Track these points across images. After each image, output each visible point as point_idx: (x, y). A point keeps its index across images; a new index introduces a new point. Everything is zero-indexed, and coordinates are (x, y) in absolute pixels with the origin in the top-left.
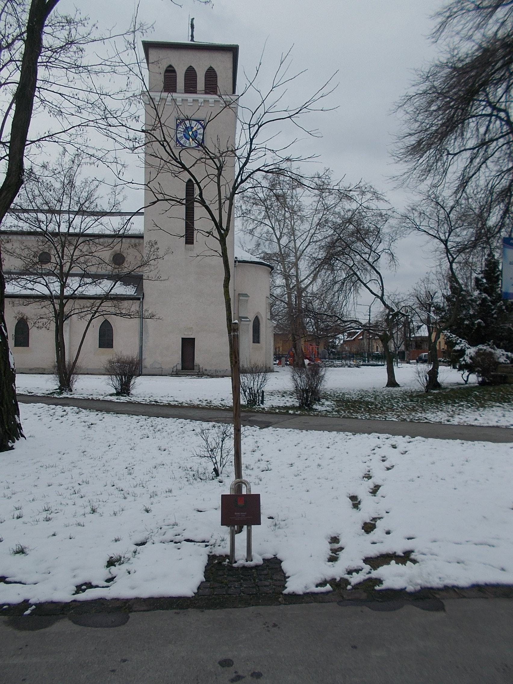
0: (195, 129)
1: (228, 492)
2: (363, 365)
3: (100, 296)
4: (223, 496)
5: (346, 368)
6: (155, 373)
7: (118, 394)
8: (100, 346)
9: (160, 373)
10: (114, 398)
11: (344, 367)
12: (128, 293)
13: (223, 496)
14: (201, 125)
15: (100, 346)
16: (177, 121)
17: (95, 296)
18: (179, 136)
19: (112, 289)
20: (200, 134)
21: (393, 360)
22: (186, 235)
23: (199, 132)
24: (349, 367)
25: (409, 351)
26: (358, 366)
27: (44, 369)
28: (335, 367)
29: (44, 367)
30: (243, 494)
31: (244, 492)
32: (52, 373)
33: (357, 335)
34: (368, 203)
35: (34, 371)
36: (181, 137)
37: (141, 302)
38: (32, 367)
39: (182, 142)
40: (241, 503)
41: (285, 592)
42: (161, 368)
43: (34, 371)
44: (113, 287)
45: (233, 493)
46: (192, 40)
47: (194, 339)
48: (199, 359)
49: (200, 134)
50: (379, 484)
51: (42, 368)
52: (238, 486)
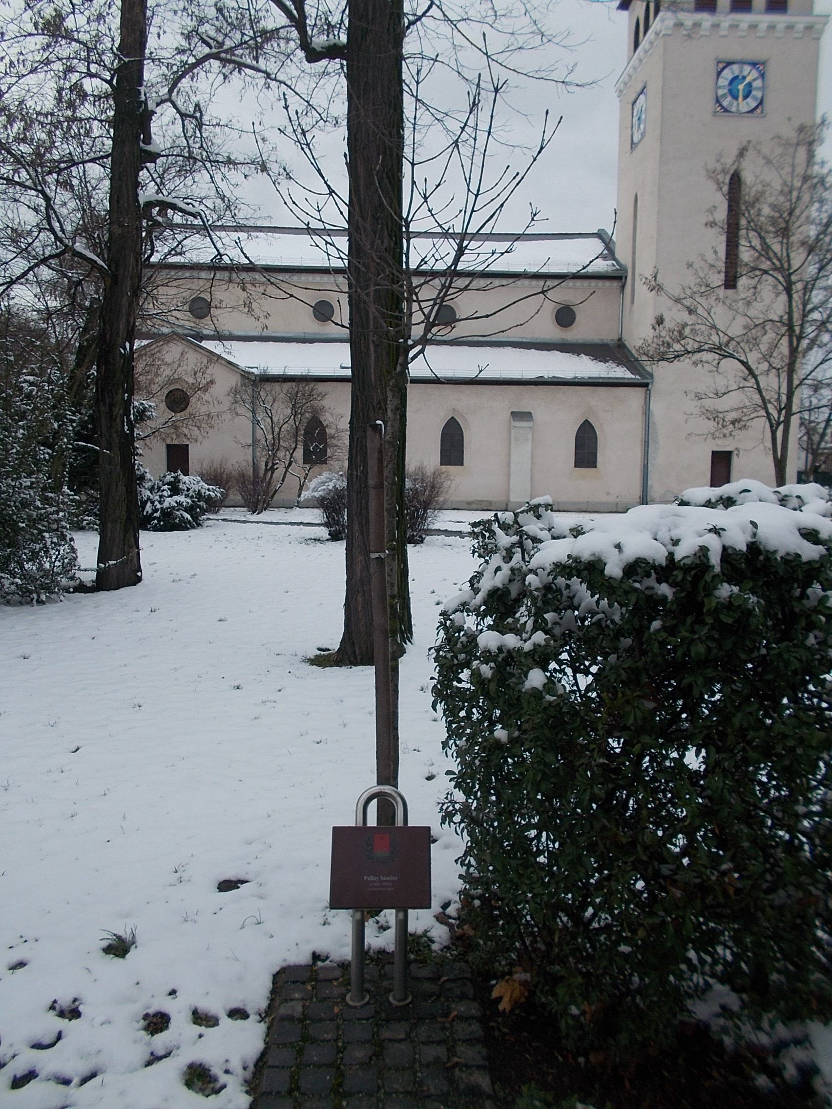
0: (748, 80)
1: (349, 820)
4: (339, 833)
13: (339, 833)
27: (490, 503)
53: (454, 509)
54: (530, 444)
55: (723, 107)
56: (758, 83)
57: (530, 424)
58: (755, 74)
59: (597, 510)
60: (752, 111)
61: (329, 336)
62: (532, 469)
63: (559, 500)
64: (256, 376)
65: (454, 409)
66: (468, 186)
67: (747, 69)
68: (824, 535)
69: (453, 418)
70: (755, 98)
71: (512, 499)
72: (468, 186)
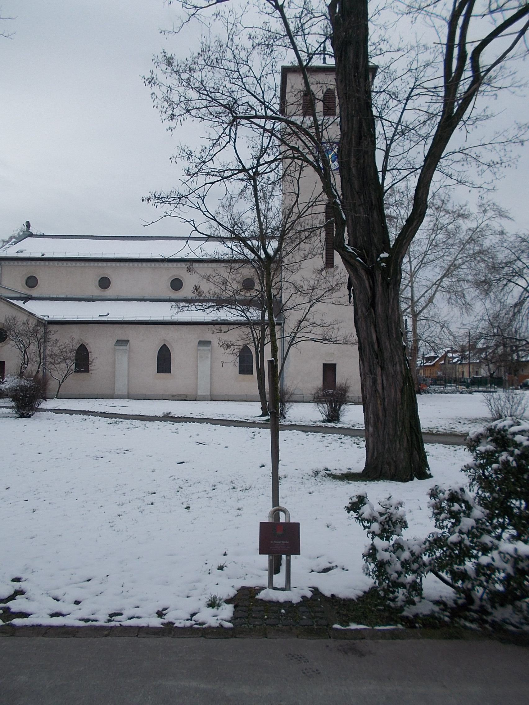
1: (266, 520)
2: (476, 391)
3: (241, 322)
4: (262, 524)
5: (458, 395)
7: (329, 421)
10: (322, 424)
11: (456, 393)
13: (262, 524)
17: (237, 322)
19: (306, 315)
24: (461, 393)
25: (518, 377)
27: (186, 396)
28: (445, 393)
29: (186, 394)
30: (281, 521)
31: (283, 519)
32: (194, 399)
33: (436, 361)
34: (490, 221)
37: (282, 327)
38: (175, 394)
40: (280, 532)
44: (307, 313)
45: (271, 521)
46: (324, 62)
47: (323, 364)
51: (185, 395)
52: (276, 514)
53: (164, 400)
54: (210, 359)
57: (209, 348)
59: (233, 400)
61: (106, 298)
62: (211, 374)
63: (229, 394)
64: (46, 321)
65: (164, 340)
66: (201, 210)
68: (2, 418)
69: (165, 345)
71: (199, 393)
72: (201, 210)
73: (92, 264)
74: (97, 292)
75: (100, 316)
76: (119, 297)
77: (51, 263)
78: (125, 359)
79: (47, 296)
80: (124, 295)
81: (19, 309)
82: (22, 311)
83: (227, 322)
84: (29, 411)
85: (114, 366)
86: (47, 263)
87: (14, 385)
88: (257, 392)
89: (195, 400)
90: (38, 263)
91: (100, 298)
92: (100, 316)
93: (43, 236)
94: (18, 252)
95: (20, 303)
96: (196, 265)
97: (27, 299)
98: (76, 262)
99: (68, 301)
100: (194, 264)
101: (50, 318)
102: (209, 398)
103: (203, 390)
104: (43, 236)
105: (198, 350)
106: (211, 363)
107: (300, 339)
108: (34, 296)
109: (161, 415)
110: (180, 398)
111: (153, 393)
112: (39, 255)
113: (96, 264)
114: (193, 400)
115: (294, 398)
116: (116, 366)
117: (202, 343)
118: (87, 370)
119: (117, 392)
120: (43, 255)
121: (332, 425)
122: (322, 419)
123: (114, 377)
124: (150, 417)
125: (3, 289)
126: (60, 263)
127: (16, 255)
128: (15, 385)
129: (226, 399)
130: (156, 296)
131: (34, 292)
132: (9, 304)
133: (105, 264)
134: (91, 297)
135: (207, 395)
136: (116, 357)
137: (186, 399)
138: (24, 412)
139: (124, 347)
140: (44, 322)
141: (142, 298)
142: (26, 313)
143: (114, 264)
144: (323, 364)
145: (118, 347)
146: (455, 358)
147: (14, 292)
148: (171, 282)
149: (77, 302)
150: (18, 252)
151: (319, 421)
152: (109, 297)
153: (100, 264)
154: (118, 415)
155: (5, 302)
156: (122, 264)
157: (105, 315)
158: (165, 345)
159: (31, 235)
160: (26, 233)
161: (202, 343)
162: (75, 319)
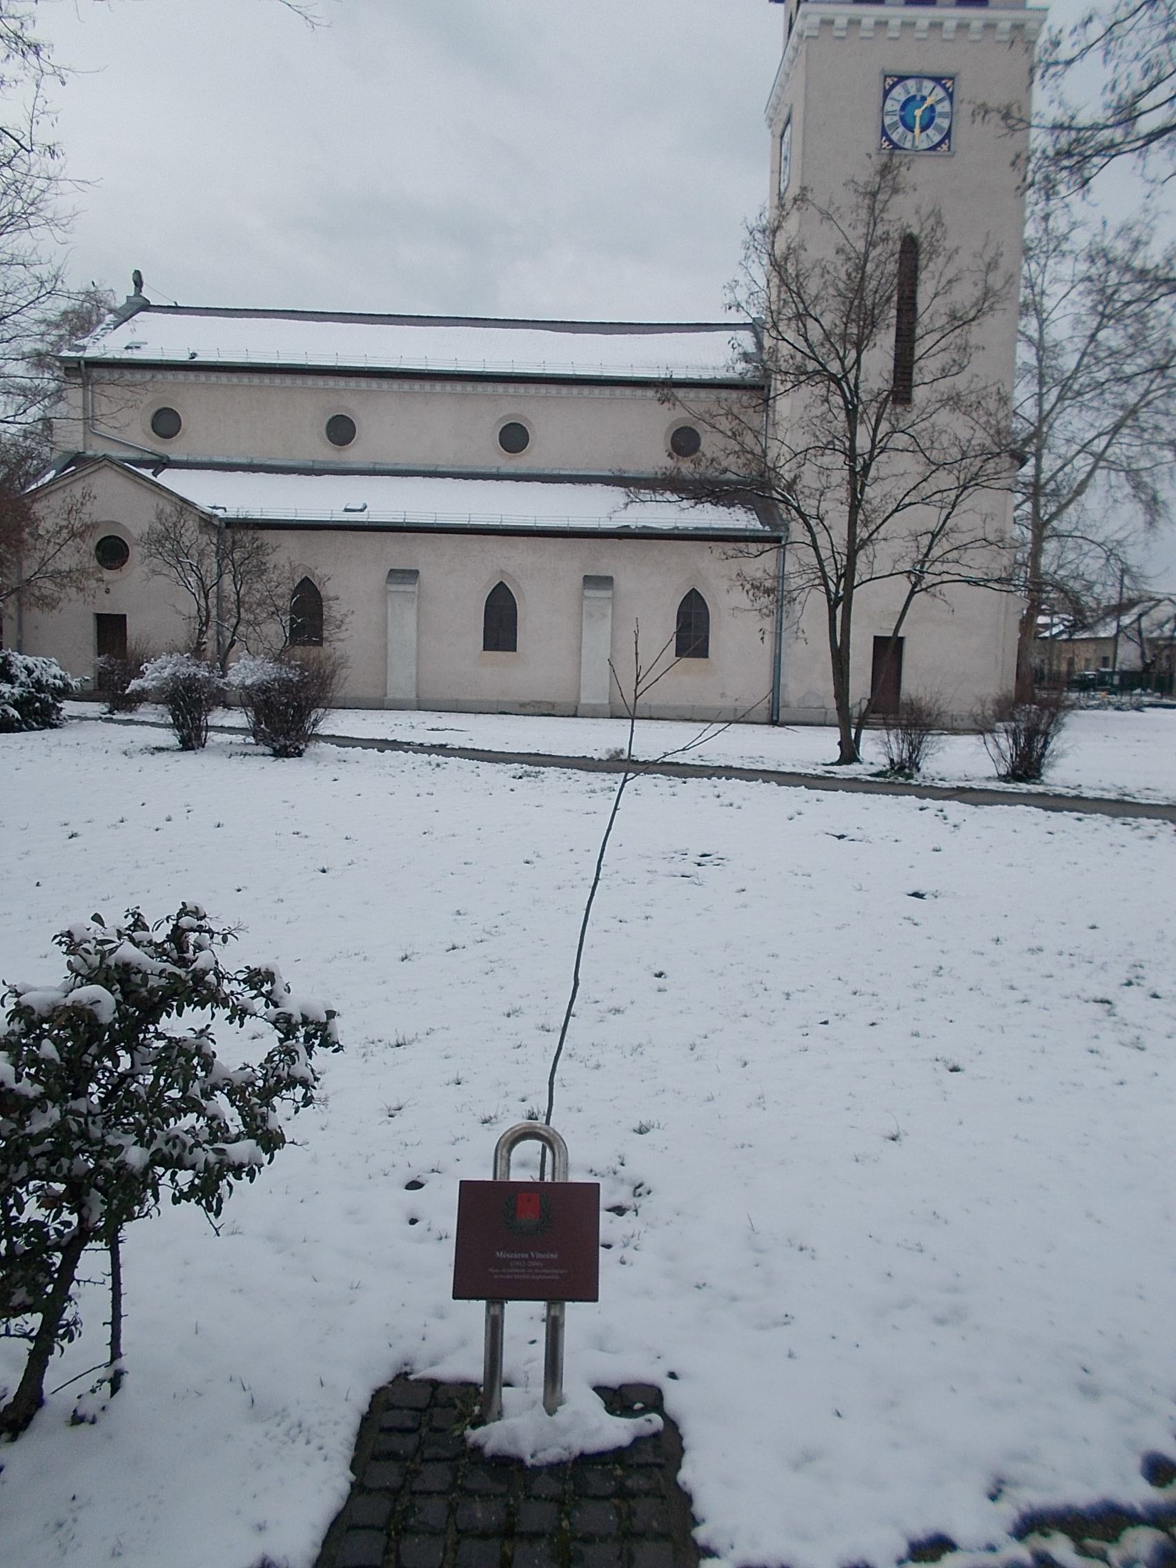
0: (929, 101)
2: (1152, 705)
5: (1111, 713)
6: (667, 717)
7: (1019, 779)
8: (486, 648)
9: (821, 719)
11: (1106, 709)
12: (741, 525)
14: (946, 90)
15: (486, 648)
16: (885, 81)
18: (888, 121)
20: (942, 115)
21: (120, 695)
22: (911, 387)
23: (939, 108)
24: (1118, 709)
26: (1139, 708)
27: (553, 705)
32: (571, 713)
35: (530, 709)
36: (894, 126)
39: (895, 137)
41: (474, 1435)
42: (823, 707)
43: (530, 709)
47: (875, 637)
48: (913, 684)
49: (942, 115)
50: (961, 1067)
51: (548, 703)
55: (941, 142)
56: (944, 107)
57: (609, 594)
58: (940, 93)
60: (933, 148)
61: (347, 466)
63: (653, 704)
64: (221, 520)
65: (502, 571)
67: (928, 85)
69: (501, 583)
70: (939, 129)
73: (310, 381)
74: (323, 451)
75: (347, 510)
76: (377, 467)
77: (213, 377)
78: (410, 617)
79: (205, 459)
80: (389, 461)
81: (153, 488)
82: (164, 494)
83: (650, 531)
84: (297, 740)
85: (384, 632)
86: (202, 377)
87: (264, 677)
88: (832, 704)
89: (575, 716)
90: (181, 376)
91: (332, 466)
92: (347, 510)
93: (176, 309)
94: (127, 348)
95: (147, 473)
96: (680, 393)
97: (161, 464)
98: (272, 376)
99: (258, 472)
100: (675, 390)
101: (231, 514)
102: (608, 711)
103: (594, 691)
104: (176, 309)
105: (583, 598)
106: (612, 629)
107: (938, 579)
108: (173, 457)
109: (601, 754)
110: (537, 710)
111: (474, 698)
112: (184, 357)
113: (320, 382)
114: (568, 716)
115: (946, 720)
116: (390, 631)
117: (397, 575)
118: (512, 647)
119: (393, 694)
120: (193, 356)
121: (1024, 787)
122: (993, 773)
123: (385, 658)
124: (491, 754)
125: (100, 438)
126: (234, 378)
127: (127, 355)
128: (267, 678)
129: (645, 716)
130: (466, 467)
131: (173, 450)
132: (129, 475)
133: (341, 382)
134: (311, 464)
135: (602, 705)
136: (389, 611)
137: (553, 712)
138: (288, 743)
139: (409, 588)
140: (216, 522)
141: (432, 469)
142: (174, 499)
143: (363, 383)
144: (875, 637)
145: (392, 588)
146: (1054, 625)
147: (123, 447)
148: (501, 433)
149: (279, 475)
150: (127, 348)
151: (988, 779)
152: (354, 466)
153: (331, 382)
154: (544, 759)
155: (118, 469)
156: (385, 384)
157: (360, 508)
158: (501, 583)
159: (147, 307)
160: (136, 299)
161: (397, 575)
162: (289, 516)
